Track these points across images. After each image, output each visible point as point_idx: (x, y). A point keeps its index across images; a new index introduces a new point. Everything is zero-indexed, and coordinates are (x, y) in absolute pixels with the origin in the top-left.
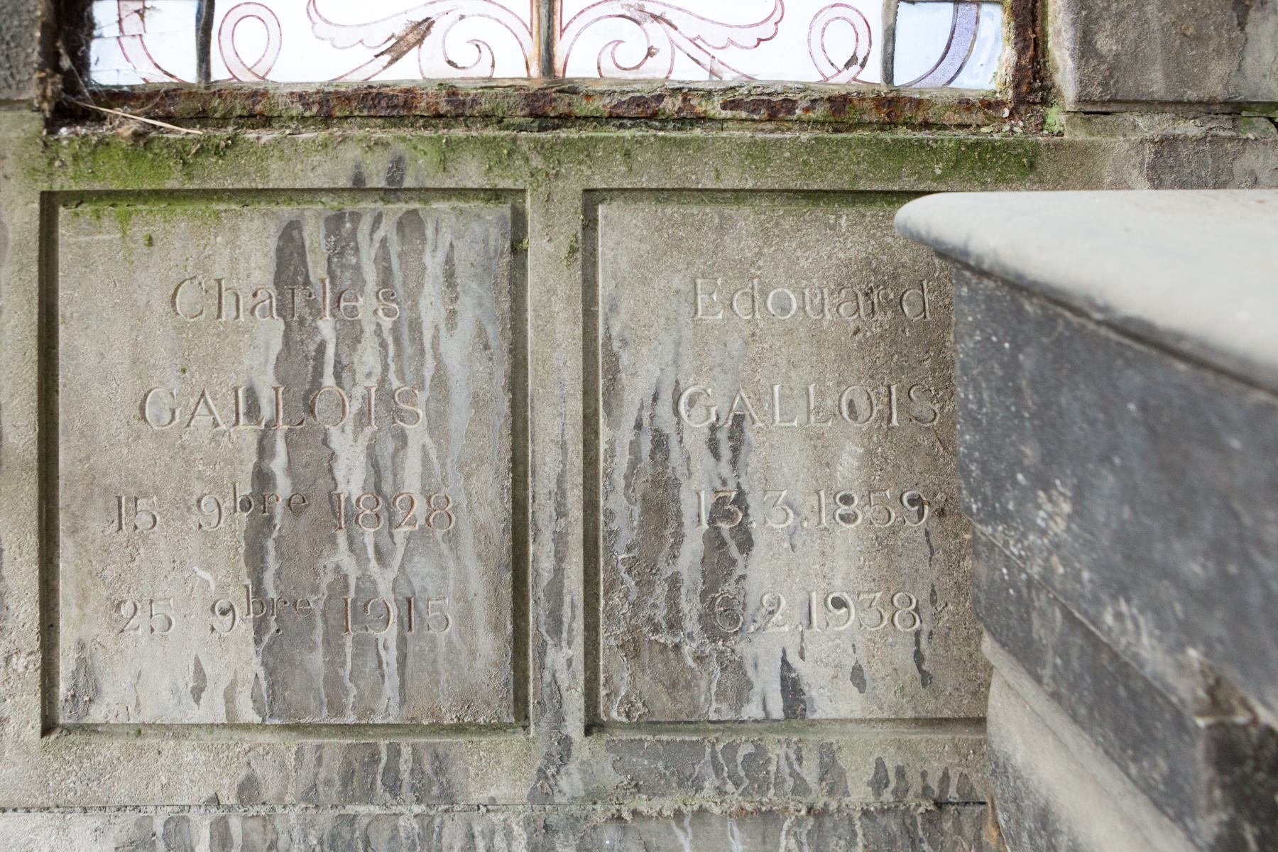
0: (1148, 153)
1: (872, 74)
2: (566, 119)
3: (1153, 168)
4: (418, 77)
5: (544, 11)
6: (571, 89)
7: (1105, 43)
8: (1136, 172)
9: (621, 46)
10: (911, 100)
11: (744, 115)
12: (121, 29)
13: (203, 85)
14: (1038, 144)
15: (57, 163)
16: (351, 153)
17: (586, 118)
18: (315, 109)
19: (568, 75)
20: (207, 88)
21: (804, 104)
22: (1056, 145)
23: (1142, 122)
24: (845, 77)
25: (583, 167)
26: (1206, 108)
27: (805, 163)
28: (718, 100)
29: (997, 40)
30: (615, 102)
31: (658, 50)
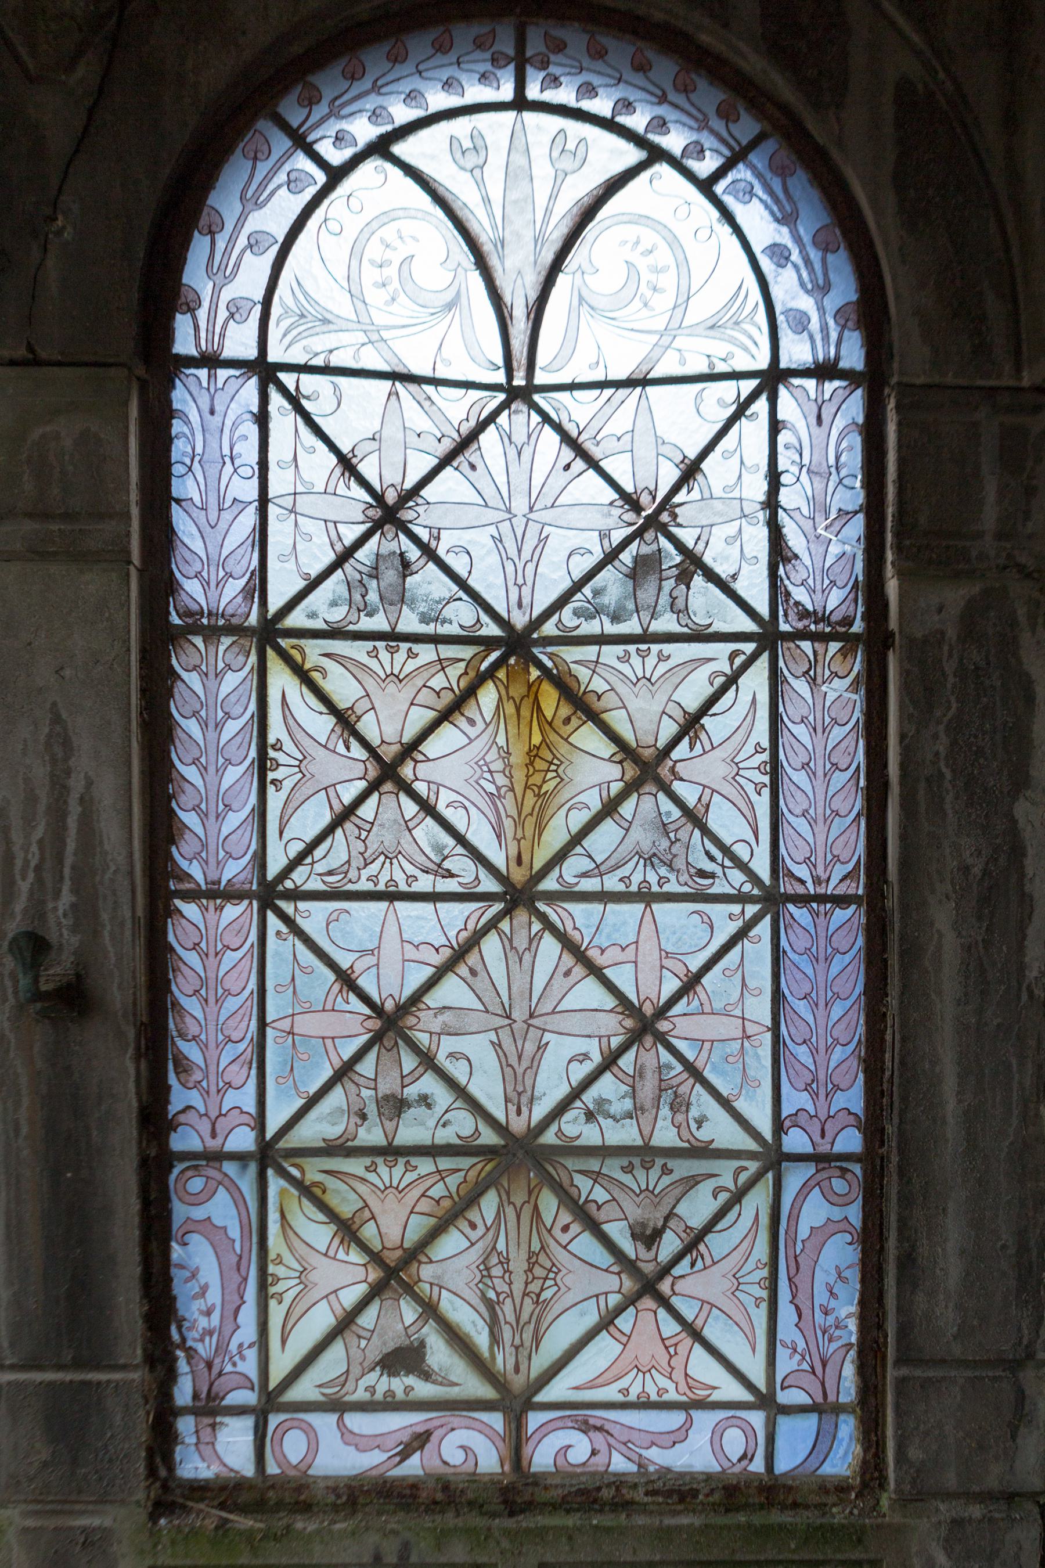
0: (943, 1531)
1: (758, 1466)
2: (530, 1507)
3: (946, 1540)
4: (421, 1472)
5: (513, 1426)
6: (537, 1480)
7: (915, 1453)
8: (934, 1544)
9: (570, 1450)
10: (784, 1486)
11: (661, 1500)
12: (198, 1438)
13: (260, 1479)
14: (865, 1526)
15: (160, 1547)
16: (372, 1539)
17: (545, 1504)
18: (344, 1498)
19: (532, 1470)
20: (263, 1482)
21: (706, 1490)
22: (878, 1526)
23: (942, 1507)
24: (737, 1469)
25: (539, 1548)
26: (986, 1497)
27: (697, 1542)
28: (641, 1490)
29: (851, 1439)
30: (566, 1492)
31: (599, 1451)
